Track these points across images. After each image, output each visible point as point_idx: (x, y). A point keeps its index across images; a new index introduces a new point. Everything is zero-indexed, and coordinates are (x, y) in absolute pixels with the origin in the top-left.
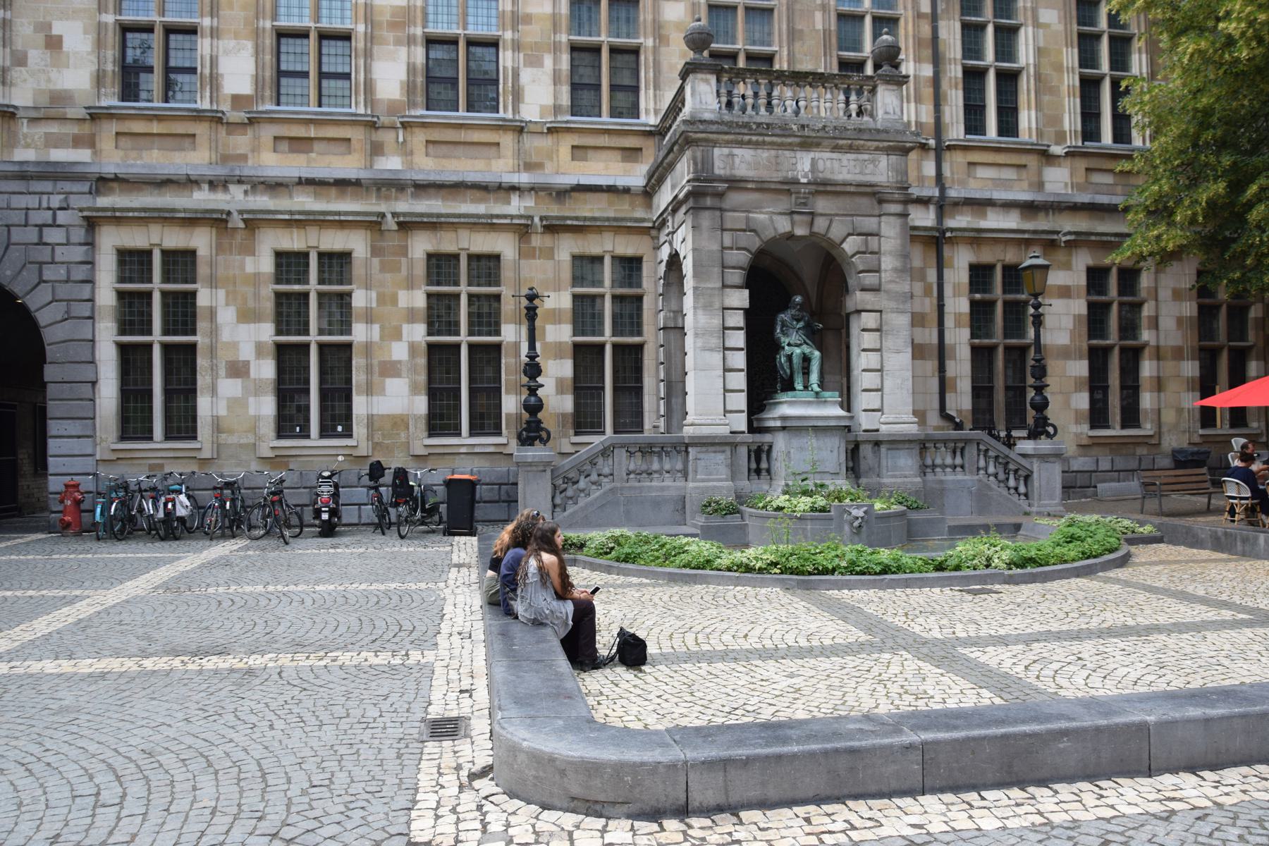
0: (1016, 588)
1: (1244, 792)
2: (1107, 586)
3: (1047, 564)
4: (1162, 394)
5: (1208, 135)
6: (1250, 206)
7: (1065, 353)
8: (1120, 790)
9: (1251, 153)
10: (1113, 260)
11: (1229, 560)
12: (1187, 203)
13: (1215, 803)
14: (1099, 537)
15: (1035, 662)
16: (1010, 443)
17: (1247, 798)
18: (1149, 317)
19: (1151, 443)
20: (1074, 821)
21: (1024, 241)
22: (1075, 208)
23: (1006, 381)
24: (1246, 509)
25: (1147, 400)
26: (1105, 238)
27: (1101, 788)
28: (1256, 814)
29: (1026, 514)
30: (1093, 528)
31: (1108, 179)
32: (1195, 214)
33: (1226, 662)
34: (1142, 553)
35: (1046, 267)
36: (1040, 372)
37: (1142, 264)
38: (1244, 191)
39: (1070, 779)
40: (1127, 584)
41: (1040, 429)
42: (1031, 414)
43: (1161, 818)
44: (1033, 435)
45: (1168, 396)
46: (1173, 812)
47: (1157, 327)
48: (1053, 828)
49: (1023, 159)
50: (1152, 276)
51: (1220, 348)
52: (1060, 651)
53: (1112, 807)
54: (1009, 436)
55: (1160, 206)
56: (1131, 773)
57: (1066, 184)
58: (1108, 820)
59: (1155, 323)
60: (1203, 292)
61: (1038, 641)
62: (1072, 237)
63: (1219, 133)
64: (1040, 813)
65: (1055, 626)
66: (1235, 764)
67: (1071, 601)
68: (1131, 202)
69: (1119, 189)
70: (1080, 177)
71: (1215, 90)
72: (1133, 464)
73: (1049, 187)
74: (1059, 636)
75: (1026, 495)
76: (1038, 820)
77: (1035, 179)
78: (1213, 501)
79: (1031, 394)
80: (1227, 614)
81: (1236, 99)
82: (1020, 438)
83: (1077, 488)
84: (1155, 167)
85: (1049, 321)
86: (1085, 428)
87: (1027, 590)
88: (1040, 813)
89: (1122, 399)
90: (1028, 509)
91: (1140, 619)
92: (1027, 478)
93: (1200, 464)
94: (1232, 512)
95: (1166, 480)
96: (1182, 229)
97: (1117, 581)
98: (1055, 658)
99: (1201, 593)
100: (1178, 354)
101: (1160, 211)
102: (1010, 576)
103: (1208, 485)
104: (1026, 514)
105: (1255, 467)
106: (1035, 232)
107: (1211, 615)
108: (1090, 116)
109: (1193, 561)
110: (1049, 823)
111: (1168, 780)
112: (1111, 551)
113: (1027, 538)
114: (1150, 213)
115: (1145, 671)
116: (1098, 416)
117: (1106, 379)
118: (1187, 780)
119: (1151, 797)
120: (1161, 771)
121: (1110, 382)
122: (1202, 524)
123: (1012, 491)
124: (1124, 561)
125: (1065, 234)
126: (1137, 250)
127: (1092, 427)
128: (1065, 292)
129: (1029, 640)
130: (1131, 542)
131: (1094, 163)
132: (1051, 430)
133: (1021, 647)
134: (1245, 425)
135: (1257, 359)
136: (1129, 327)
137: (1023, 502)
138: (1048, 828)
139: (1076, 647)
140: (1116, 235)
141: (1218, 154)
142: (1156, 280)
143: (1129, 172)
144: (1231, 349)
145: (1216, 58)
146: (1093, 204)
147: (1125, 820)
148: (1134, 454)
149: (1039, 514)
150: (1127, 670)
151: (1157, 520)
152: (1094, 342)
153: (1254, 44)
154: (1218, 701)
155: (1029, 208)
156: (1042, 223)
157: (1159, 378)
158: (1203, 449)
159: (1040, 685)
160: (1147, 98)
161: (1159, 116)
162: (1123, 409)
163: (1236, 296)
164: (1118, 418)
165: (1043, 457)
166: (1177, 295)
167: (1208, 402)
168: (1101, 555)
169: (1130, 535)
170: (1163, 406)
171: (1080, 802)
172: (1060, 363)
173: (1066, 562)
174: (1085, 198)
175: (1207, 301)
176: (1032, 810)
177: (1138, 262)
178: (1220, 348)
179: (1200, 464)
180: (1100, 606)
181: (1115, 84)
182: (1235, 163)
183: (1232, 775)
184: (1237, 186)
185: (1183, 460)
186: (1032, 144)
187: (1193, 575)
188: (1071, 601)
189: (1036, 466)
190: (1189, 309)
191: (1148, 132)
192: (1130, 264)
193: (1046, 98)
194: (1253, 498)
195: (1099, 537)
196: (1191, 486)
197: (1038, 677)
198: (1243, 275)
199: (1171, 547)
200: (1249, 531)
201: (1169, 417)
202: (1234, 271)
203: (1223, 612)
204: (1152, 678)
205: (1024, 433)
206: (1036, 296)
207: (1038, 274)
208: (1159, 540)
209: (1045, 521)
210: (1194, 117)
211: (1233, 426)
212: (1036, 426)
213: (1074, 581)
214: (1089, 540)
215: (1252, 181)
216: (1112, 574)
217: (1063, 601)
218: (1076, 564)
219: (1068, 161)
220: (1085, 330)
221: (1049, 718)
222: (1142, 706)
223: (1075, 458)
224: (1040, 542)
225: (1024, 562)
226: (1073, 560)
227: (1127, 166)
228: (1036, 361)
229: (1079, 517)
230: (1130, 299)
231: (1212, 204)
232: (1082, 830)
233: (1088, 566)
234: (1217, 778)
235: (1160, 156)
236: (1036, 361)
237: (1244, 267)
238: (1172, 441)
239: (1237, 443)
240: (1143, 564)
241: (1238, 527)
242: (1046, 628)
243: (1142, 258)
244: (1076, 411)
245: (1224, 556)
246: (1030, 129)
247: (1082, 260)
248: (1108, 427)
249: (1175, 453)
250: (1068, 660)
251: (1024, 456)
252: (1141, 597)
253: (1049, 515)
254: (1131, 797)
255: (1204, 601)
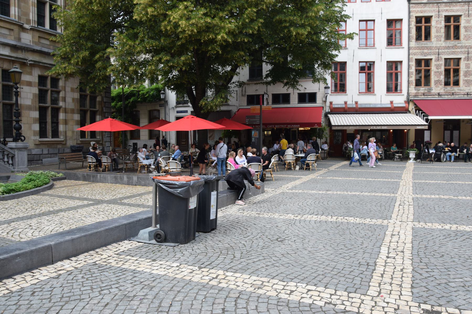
0: (6, 202)
1: (85, 261)
2: (44, 197)
3: (20, 191)
4: (67, 126)
5: (83, 34)
6: (96, 62)
7: (29, 108)
8: (41, 272)
9: (98, 43)
10: (48, 74)
11: (88, 184)
12: (75, 57)
13: (75, 268)
14: (41, 179)
15: (11, 230)
16: (5, 143)
17: (86, 263)
18: (62, 97)
19: (63, 143)
20: (22, 288)
21: (13, 61)
22: (34, 51)
23: (3, 118)
24: (95, 166)
25: (61, 128)
26: (46, 65)
27: (33, 273)
28: (88, 268)
29: (12, 172)
30: (40, 176)
31: (47, 42)
32: (78, 62)
33: (84, 219)
34: (58, 184)
35: (20, 73)
36: (19, 115)
37: (59, 77)
38: (95, 56)
39: (21, 272)
40: (51, 195)
41: (18, 137)
42: (14, 131)
43: (56, 278)
44: (15, 140)
45: (69, 126)
46: (60, 275)
47: (65, 101)
48: (12, 293)
49: (12, 27)
50: (64, 82)
51: (87, 111)
52: (22, 224)
53: (38, 279)
54: (5, 141)
55: (66, 56)
56: (45, 265)
57: (30, 41)
58: (35, 284)
59: (64, 99)
60: (82, 90)
61: (13, 222)
62: (33, 63)
63: (87, 34)
64: (7, 289)
65: (21, 215)
66: (83, 253)
67: (29, 204)
68: (56, 53)
69: (52, 47)
70: (36, 40)
71: (86, 18)
72: (56, 151)
73: (23, 41)
74: (22, 219)
75: (12, 164)
76: (7, 292)
77: (17, 36)
78: (84, 164)
79: (14, 123)
80: (86, 202)
81: (93, 23)
82: (9, 141)
83: (34, 161)
84: (65, 41)
85: (23, 95)
86: (37, 138)
87: (10, 202)
88: (7, 289)
89: (52, 127)
90: (13, 170)
91: (55, 208)
92: (13, 158)
93: (80, 151)
94: (90, 167)
95: (67, 157)
96: (74, 66)
97: (48, 195)
98: (20, 227)
99: (78, 196)
100: (73, 111)
101: (66, 58)
102: (3, 197)
103: (82, 158)
104: (12, 172)
105: (97, 152)
106: (17, 58)
107: (80, 203)
108: (41, 17)
109: (76, 185)
110: (12, 292)
111: (59, 264)
112: (46, 184)
113: (12, 181)
114: (62, 58)
115: (55, 226)
116: (43, 133)
117: (46, 119)
118: (67, 261)
119: (52, 271)
120: (56, 262)
121: (48, 120)
122: (80, 172)
123: (6, 163)
124: (51, 187)
125: (30, 61)
126: (57, 71)
127: (40, 137)
128: (29, 84)
129: (9, 222)
130: (54, 180)
131: (42, 35)
132: (23, 138)
133: (6, 225)
134: (95, 137)
135: (99, 115)
136: (55, 101)
137: (11, 167)
138: (11, 294)
139: (29, 222)
140: (50, 64)
141: (86, 41)
142: (65, 84)
143: (55, 41)
144: (91, 111)
145: (86, 6)
146: (41, 51)
147: (42, 282)
148: (56, 148)
149: (18, 172)
150: (48, 227)
151: (64, 171)
152: (41, 105)
153: (99, 5)
154: (77, 232)
155: (14, 48)
156: (20, 55)
157: (66, 120)
158: (81, 145)
159: (13, 239)
160: (62, 15)
161: (66, 23)
162: (52, 131)
163: (91, 92)
164: (50, 134)
165: (19, 149)
166: (72, 90)
167: (83, 129)
168: (42, 186)
169: (54, 177)
170: (67, 130)
171: (25, 280)
172: (27, 112)
173: (28, 189)
174: (38, 48)
175: (83, 93)
176: (4, 288)
177: (57, 76)
178: (87, 111)
179: (80, 151)
180: (40, 205)
181: (51, 6)
182: (92, 46)
183: (81, 257)
184: (93, 54)
185: (75, 150)
186: (16, 22)
187: (75, 190)
188: (29, 204)
189: (16, 153)
190: (77, 95)
191: (63, 28)
192: (54, 76)
193: (22, 4)
194: (96, 162)
195: (41, 179)
196: (77, 159)
197: (12, 236)
198: (94, 85)
199: (69, 181)
200: (95, 173)
201: (69, 134)
202: (91, 84)
203: (85, 202)
204: (58, 228)
205: (11, 139)
206: (16, 84)
207: (17, 75)
208: (64, 179)
209: (20, 174)
210: (79, 26)
211: (91, 138)
212: (16, 136)
213: (30, 197)
214: (37, 180)
215: (97, 53)
216: (46, 193)
217: (26, 205)
218: (32, 190)
219: (31, 32)
220: (37, 99)
221: (12, 251)
222: (50, 239)
223: (33, 149)
224: (17, 183)
225: (9, 191)
226: (31, 189)
227: (54, 39)
228: (16, 110)
229: (34, 172)
230: (55, 89)
231: (84, 59)
232: (25, 291)
233: (37, 190)
234: (77, 259)
235: (66, 38)
236: (16, 110)
237: (94, 83)
238: (71, 143)
239: (92, 143)
240: (58, 188)
241: (92, 172)
242: (17, 216)
243: (59, 74)
244: (34, 131)
245: (87, 182)
246: (15, 15)
247: (37, 72)
248: (47, 137)
249: (72, 147)
250: (25, 227)
251: (11, 148)
252: (56, 200)
253: (22, 172)
254: (44, 273)
255: (79, 199)
